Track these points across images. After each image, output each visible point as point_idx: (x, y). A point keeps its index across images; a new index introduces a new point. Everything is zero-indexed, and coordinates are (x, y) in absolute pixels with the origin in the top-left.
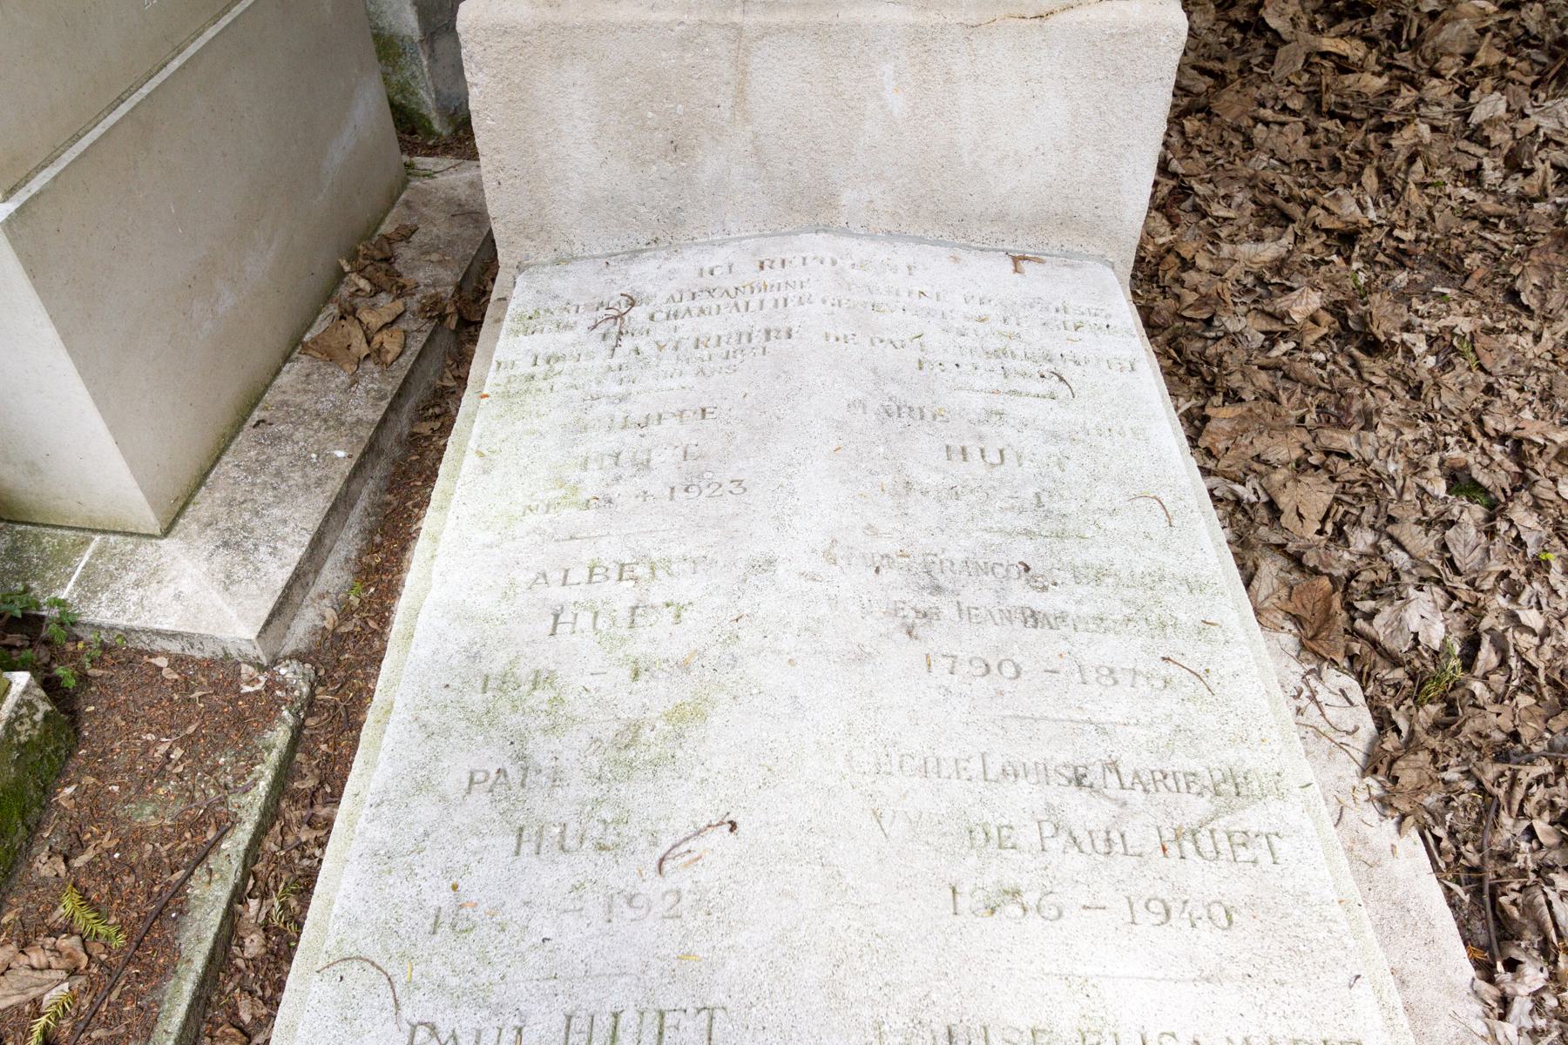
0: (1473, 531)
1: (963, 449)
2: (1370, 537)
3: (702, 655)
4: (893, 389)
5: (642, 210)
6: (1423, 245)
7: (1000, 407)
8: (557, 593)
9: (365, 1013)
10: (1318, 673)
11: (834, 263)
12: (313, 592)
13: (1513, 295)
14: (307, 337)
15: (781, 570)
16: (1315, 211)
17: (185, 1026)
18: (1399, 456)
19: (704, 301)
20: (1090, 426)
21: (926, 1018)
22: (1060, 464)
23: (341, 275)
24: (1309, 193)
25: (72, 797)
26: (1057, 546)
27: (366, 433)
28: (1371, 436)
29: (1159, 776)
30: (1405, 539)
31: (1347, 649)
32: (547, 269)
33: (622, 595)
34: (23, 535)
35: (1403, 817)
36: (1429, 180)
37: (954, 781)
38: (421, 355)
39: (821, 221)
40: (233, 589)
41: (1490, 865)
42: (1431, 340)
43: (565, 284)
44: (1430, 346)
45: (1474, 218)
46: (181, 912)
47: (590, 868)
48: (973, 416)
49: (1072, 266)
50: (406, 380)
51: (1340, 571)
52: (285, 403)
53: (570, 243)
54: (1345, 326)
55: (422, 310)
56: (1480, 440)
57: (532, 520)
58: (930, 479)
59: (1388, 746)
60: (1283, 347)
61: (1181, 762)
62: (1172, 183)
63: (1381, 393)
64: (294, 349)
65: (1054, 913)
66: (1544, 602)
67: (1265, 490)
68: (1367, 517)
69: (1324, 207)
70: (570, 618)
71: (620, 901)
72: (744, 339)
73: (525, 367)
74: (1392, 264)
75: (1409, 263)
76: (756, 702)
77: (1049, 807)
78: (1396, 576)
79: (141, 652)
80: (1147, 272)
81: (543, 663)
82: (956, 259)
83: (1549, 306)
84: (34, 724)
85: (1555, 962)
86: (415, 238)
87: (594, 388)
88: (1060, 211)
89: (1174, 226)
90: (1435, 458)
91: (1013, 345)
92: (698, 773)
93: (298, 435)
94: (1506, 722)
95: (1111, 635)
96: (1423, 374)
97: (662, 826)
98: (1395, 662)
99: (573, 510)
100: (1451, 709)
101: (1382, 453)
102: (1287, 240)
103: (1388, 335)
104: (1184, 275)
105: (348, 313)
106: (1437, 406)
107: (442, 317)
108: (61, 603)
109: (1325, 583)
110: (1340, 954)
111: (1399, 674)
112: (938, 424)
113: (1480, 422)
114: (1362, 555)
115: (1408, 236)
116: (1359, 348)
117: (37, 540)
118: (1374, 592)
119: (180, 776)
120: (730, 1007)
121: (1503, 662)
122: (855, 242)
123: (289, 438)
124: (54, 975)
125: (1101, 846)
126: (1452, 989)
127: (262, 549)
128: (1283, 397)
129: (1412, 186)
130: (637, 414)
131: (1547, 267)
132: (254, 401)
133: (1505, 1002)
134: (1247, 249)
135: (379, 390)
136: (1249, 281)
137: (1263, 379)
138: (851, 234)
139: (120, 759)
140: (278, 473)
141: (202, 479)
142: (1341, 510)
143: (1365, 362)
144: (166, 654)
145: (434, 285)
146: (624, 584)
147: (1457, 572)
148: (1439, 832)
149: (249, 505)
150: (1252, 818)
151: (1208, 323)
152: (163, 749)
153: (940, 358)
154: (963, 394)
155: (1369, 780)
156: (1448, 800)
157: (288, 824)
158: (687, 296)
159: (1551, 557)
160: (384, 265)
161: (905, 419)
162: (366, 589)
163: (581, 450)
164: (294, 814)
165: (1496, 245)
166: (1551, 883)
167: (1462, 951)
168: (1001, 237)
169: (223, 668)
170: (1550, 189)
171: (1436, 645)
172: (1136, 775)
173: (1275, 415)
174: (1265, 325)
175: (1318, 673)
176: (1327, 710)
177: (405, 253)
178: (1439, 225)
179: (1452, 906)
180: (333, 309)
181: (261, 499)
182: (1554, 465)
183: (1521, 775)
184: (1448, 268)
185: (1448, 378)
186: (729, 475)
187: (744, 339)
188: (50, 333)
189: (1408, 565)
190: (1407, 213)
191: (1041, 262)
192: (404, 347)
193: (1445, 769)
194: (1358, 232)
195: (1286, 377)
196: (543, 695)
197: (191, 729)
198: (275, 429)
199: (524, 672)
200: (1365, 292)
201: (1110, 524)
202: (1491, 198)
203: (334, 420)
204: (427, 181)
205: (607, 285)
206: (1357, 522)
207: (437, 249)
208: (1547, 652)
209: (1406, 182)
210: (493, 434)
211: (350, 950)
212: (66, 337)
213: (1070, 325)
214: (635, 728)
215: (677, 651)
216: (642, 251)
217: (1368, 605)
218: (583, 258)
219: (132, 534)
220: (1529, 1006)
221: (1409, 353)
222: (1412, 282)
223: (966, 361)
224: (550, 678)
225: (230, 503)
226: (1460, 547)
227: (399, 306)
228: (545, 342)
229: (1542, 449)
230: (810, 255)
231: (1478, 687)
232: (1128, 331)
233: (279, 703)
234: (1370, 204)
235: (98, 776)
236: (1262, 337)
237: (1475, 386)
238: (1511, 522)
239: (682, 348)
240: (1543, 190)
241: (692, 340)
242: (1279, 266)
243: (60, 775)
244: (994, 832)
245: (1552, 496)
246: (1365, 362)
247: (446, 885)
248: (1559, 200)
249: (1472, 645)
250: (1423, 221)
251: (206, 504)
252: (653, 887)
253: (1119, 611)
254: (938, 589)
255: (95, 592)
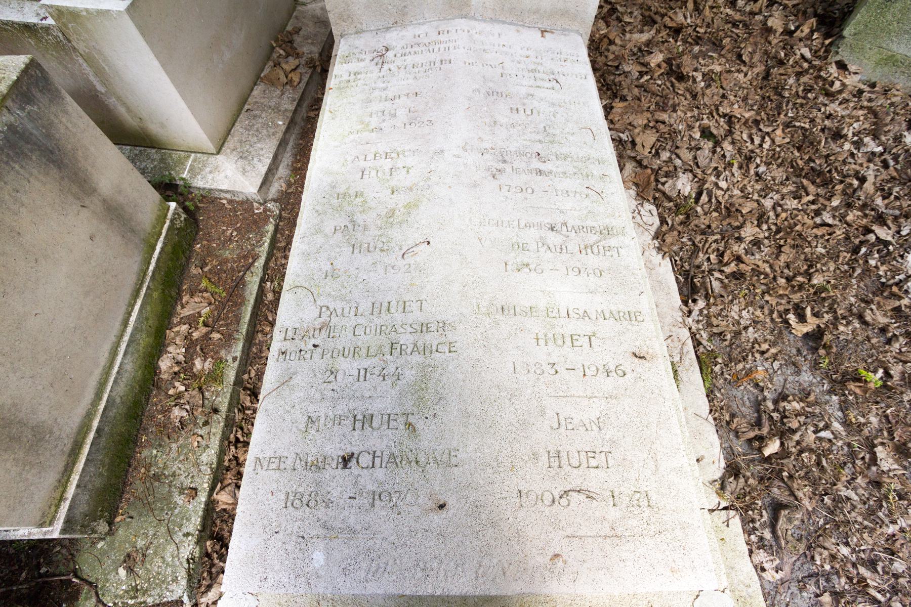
0: (707, 151)
1: (517, 109)
2: (668, 154)
3: (417, 185)
4: (491, 85)
5: (390, 7)
6: (707, 35)
7: (532, 92)
8: (362, 164)
9: (304, 303)
10: (642, 205)
11: (469, 32)
12: (276, 177)
13: (740, 56)
14: (262, 75)
15: (446, 154)
16: (666, 19)
17: (250, 320)
18: (684, 123)
19: (416, 49)
20: (567, 101)
21: (494, 303)
22: (554, 116)
23: (274, 48)
24: (665, 11)
25: (200, 248)
26: (551, 146)
27: (290, 115)
28: (675, 115)
29: (581, 228)
30: (681, 155)
31: (654, 195)
32: (353, 36)
33: (387, 164)
34: (165, 153)
35: (665, 253)
36: (714, 5)
37: (508, 228)
38: (308, 84)
39: (464, 13)
40: (247, 174)
41: (693, 269)
42: (704, 75)
43: (360, 42)
44: (703, 78)
45: (730, 22)
46: (244, 286)
47: (379, 257)
48: (522, 96)
49: (565, 35)
50: (303, 93)
51: (655, 167)
52: (256, 102)
53: (361, 24)
54: (671, 69)
55: (306, 64)
56: (716, 117)
57: (352, 137)
58: (504, 121)
59: (663, 229)
60: (646, 78)
61: (590, 223)
62: (609, 7)
63: (681, 97)
64: (258, 80)
65: (540, 271)
66: (729, 178)
67: (631, 136)
68: (668, 147)
69: (670, 17)
70: (368, 173)
71: (389, 267)
72: (432, 64)
73: (346, 77)
74: (693, 42)
75: (700, 43)
76: (437, 201)
77: (541, 237)
78: (676, 169)
79: (216, 198)
80: (595, 46)
81: (358, 189)
82: (518, 31)
83: (753, 61)
84: (181, 222)
85: (709, 301)
86: (301, 33)
87: (373, 85)
88: (562, 8)
89: (608, 26)
90: (698, 124)
91: (539, 68)
92: (416, 225)
93: (263, 115)
94: (707, 222)
95: (568, 179)
96: (699, 89)
97: (403, 243)
98: (670, 199)
99: (367, 133)
100: (688, 217)
101: (678, 122)
102: (653, 32)
103: (688, 73)
104: (610, 47)
105: (277, 64)
106: (702, 103)
107: (314, 67)
108: (184, 179)
109: (649, 171)
110: (638, 285)
111: (671, 204)
112: (508, 99)
113: (717, 110)
114: (664, 161)
115: (702, 30)
116: (675, 79)
117: (170, 155)
118: (667, 175)
119: (237, 241)
120: (428, 299)
121: (710, 201)
122: (477, 23)
123: (260, 116)
124: (203, 304)
125: (558, 250)
126: (673, 308)
127: (255, 159)
128: (643, 99)
129: (707, 7)
130: (391, 95)
131: (756, 44)
132: (244, 101)
133: (690, 312)
134: (636, 36)
135: (292, 98)
136: (635, 50)
137: (636, 91)
138: (476, 20)
139: (215, 236)
140: (257, 130)
141: (228, 132)
142: (659, 144)
143: (677, 84)
144: (226, 199)
145: (311, 53)
146: (387, 160)
147: (698, 167)
148: (677, 258)
149: (248, 143)
150: (613, 242)
151: (617, 67)
152: (229, 232)
153: (510, 72)
154: (518, 87)
155: (655, 241)
156: (682, 248)
157: (277, 258)
158: (409, 46)
159: (735, 162)
160: (289, 44)
161: (495, 97)
162: (296, 176)
163: (369, 110)
164: (279, 255)
165: (737, 34)
166: (713, 275)
167: (678, 296)
168: (537, 21)
169: (247, 204)
170: (764, 8)
171: (686, 194)
172: (573, 227)
173: (639, 106)
174: (639, 68)
175: (642, 205)
176: (643, 217)
177: (298, 39)
178: (715, 26)
179: (677, 283)
180: (271, 63)
181: (252, 140)
182: (743, 126)
183: (709, 239)
184: (716, 45)
185: (708, 91)
186: (427, 119)
187: (432, 64)
188: (156, 63)
189: (681, 165)
190: (703, 20)
191: (553, 33)
192: (301, 80)
193: (682, 238)
194: (682, 28)
195: (645, 90)
196: (359, 200)
197: (238, 225)
198: (254, 113)
199: (352, 192)
200: (682, 53)
201: (571, 138)
202: (738, 14)
203: (277, 109)
204: (304, 7)
205: (378, 43)
206: (664, 149)
207: (310, 38)
208: (726, 197)
209: (705, 6)
210: (335, 104)
211: (297, 284)
212: (163, 65)
213: (562, 59)
214: (393, 211)
215: (408, 184)
216: (391, 28)
217: (664, 179)
218: (367, 31)
219: (205, 153)
220: (698, 313)
221: (694, 81)
222: (700, 51)
223: (520, 74)
224: (362, 194)
225: (241, 142)
226: (701, 158)
227: (297, 62)
228: (354, 66)
229: (739, 119)
230: (459, 28)
231: (699, 209)
232: (585, 63)
233: (269, 216)
234: (689, 16)
235: (208, 241)
236: (638, 74)
237: (718, 95)
238: (722, 148)
239: (408, 68)
240: (761, 10)
241: (411, 65)
242: (649, 43)
243: (193, 241)
244: (521, 245)
245: (739, 138)
246: (677, 84)
247: (329, 263)
248: (766, 14)
249: (699, 194)
250: (709, 24)
251: (231, 142)
252: (401, 263)
253: (571, 170)
254: (505, 161)
255: (195, 175)
